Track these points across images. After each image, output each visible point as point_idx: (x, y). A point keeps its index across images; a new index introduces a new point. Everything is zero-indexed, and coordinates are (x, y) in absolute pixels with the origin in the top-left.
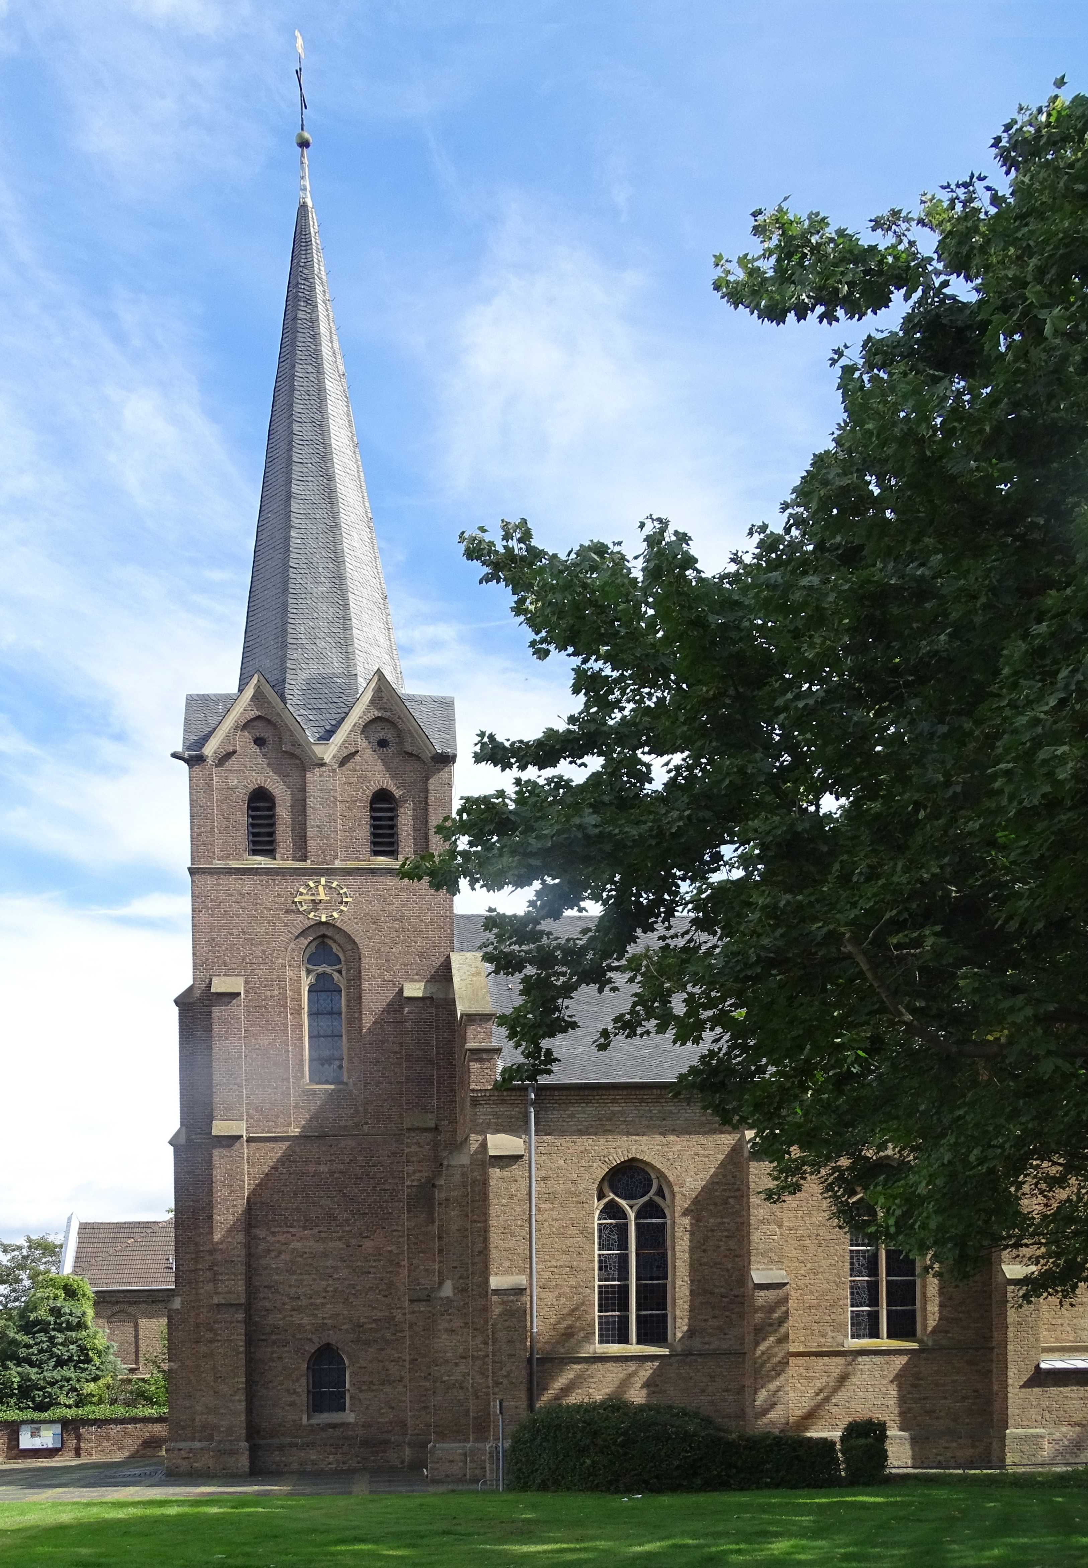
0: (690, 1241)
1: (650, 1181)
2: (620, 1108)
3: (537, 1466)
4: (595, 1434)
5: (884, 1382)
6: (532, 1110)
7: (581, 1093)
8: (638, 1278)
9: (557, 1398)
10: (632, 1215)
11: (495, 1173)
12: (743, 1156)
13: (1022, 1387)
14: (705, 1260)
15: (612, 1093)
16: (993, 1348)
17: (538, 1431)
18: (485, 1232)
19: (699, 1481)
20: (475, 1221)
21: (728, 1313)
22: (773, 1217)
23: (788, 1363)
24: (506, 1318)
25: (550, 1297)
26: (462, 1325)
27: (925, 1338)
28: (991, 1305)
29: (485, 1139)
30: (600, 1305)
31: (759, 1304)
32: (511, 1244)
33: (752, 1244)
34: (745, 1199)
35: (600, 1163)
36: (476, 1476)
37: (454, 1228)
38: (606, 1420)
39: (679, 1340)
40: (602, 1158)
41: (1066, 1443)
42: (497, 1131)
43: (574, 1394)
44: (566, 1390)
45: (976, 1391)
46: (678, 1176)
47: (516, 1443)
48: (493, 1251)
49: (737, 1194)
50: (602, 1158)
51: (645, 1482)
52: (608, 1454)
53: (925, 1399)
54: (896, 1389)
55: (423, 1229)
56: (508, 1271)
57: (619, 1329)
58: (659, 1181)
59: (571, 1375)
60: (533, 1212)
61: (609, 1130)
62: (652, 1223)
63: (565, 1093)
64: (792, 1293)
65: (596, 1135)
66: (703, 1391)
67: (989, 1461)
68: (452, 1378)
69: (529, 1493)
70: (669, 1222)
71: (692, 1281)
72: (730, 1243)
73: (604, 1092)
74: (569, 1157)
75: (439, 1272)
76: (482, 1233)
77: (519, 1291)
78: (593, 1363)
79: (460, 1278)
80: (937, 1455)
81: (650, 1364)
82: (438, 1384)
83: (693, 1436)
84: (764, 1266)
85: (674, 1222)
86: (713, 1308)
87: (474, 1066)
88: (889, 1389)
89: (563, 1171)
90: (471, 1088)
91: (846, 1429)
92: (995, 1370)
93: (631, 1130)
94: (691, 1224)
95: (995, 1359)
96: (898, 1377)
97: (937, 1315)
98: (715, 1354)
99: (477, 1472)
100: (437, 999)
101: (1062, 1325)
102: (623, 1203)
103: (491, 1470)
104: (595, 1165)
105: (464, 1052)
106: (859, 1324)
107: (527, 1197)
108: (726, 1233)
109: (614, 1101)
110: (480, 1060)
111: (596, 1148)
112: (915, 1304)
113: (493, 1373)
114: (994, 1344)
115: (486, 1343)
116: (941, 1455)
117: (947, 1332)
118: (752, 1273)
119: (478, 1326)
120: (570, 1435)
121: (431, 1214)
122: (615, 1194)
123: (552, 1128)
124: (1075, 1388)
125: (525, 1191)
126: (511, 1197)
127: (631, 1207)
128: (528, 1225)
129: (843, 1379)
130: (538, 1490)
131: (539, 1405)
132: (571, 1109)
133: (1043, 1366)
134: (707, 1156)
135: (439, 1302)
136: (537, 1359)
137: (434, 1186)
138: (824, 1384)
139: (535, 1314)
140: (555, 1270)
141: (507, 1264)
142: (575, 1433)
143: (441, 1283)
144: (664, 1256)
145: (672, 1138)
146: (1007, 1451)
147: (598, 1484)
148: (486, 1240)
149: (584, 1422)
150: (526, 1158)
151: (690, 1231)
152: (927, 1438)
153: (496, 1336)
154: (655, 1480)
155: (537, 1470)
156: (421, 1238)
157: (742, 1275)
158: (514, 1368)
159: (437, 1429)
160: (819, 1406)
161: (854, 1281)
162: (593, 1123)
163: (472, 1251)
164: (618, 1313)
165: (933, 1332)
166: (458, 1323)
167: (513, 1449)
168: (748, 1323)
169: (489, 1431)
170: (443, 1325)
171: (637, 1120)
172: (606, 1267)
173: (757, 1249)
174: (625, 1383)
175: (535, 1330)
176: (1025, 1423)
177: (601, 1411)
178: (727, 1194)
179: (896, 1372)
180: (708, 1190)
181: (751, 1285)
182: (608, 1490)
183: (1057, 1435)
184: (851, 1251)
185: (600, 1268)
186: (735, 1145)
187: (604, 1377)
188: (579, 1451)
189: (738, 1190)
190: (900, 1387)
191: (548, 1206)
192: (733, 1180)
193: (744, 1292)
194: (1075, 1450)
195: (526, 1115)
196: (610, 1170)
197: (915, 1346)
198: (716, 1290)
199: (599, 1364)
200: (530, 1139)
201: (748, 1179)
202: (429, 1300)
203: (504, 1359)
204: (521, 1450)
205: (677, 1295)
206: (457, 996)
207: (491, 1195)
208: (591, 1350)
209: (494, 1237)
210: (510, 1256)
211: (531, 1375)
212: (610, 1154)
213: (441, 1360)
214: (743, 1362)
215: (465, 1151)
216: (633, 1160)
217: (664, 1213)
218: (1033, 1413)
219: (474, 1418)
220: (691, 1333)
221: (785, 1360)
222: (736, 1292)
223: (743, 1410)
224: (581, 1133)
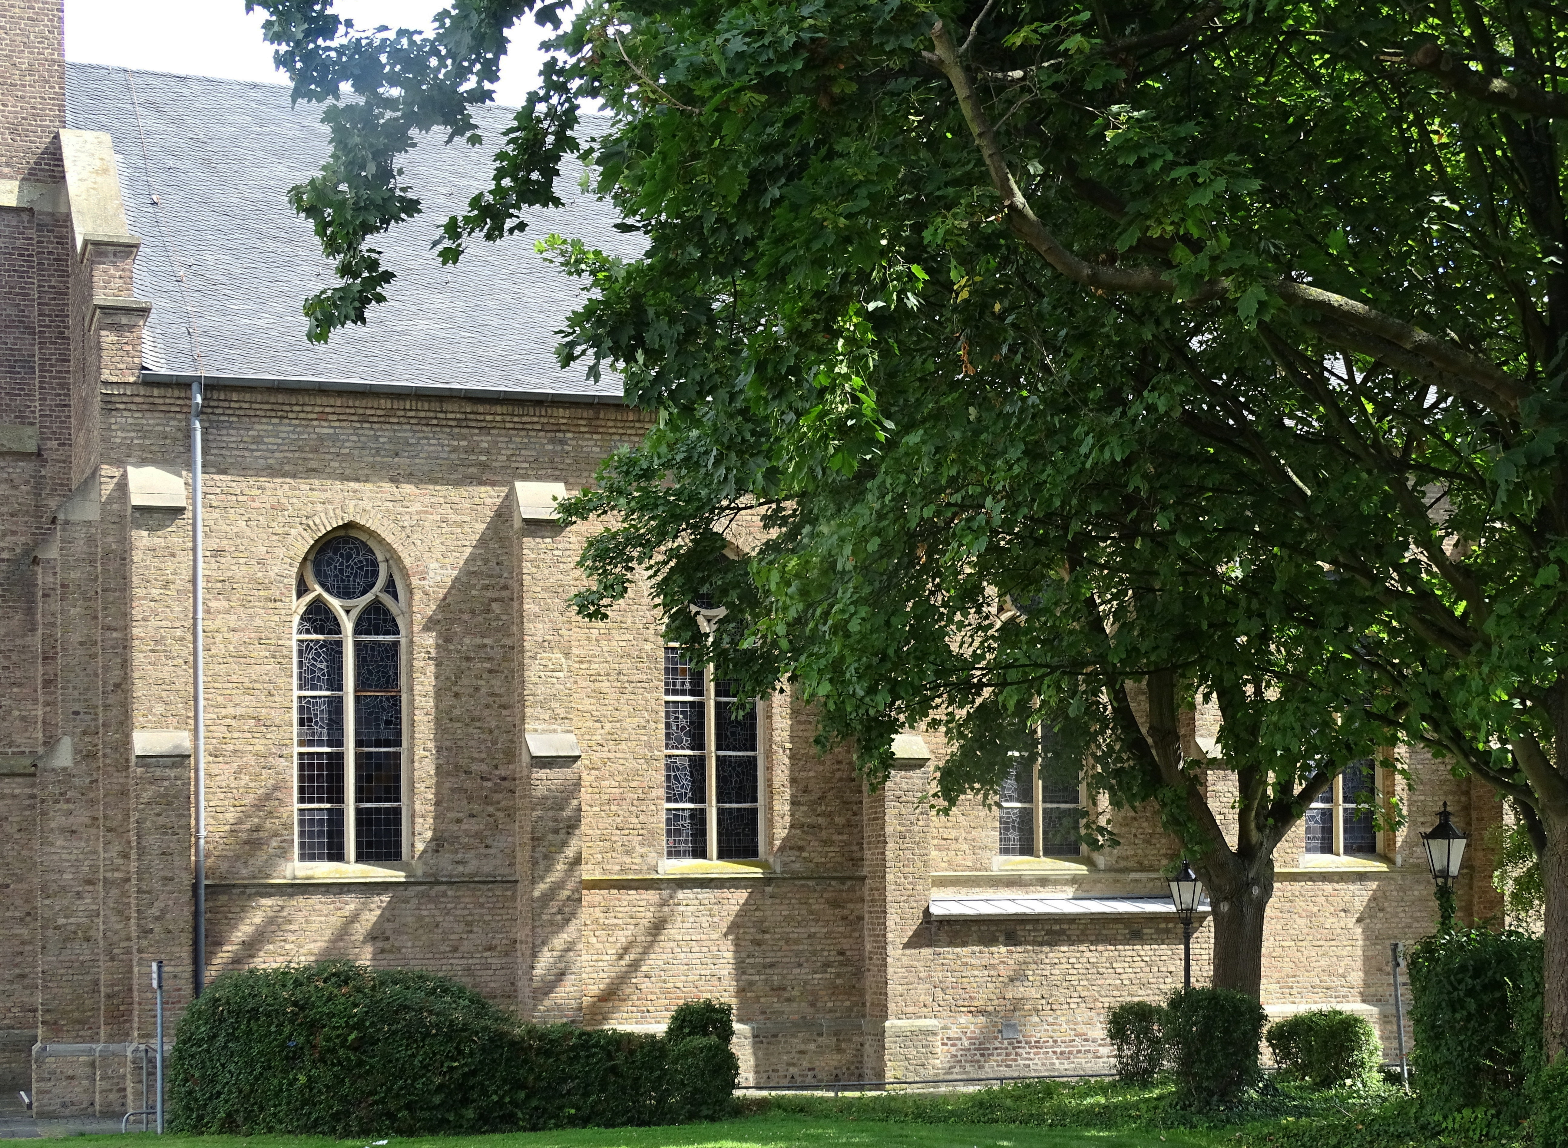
0: (436, 678)
1: (375, 564)
2: (331, 431)
3: (219, 1087)
4: (313, 1026)
5: (715, 936)
6: (198, 424)
7: (273, 400)
8: (359, 743)
9: (236, 961)
10: (348, 625)
11: (141, 538)
12: (512, 526)
13: (907, 946)
14: (457, 712)
15: (319, 401)
16: (863, 879)
17: (222, 1020)
18: (124, 647)
19: (470, 1113)
20: (109, 628)
21: (491, 809)
22: (557, 638)
23: (580, 900)
24: (158, 809)
25: (225, 772)
26: (88, 821)
27: (771, 860)
28: (861, 802)
29: (124, 476)
30: (302, 790)
31: (539, 794)
32: (166, 672)
33: (528, 686)
34: (515, 604)
35: (300, 529)
36: (110, 1105)
37: (75, 638)
38: (329, 999)
39: (420, 858)
40: (304, 521)
41: (966, 1043)
42: (143, 462)
43: (262, 954)
44: (252, 946)
45: (841, 953)
46: (417, 559)
47: (185, 1042)
48: (139, 684)
49: (505, 594)
50: (304, 521)
51: (391, 1116)
52: (333, 1064)
53: (772, 965)
54: (732, 948)
55: (18, 642)
56: (160, 724)
57: (330, 834)
58: (389, 567)
59: (257, 918)
60: (200, 615)
61: (314, 470)
62: (378, 643)
63: (248, 397)
64: (584, 776)
65: (294, 476)
66: (455, 949)
67: (860, 1076)
68: (71, 920)
69: (206, 1137)
70: (403, 641)
71: (439, 749)
72: (493, 682)
73: (306, 399)
74: (254, 516)
75: (44, 722)
76: (120, 650)
77: (179, 759)
78: (291, 895)
79: (84, 733)
80: (790, 1064)
81: (376, 899)
82: (50, 932)
83: (463, 1030)
84: (544, 726)
85: (412, 641)
86: (470, 799)
87: (108, 337)
88: (722, 948)
89: (245, 541)
90: (103, 378)
91: (674, 1019)
92: (867, 916)
93: (348, 472)
94: (438, 646)
95: (867, 898)
96: (734, 927)
97: (788, 819)
98: (471, 882)
99: (112, 1097)
100: (41, 213)
101: (957, 840)
102: (335, 603)
103: (138, 1094)
104: (293, 532)
105: (91, 308)
106: (678, 832)
107: (190, 586)
108: (487, 665)
109: (322, 417)
110: (117, 328)
111: (295, 501)
112: (755, 800)
113: (138, 911)
114: (865, 871)
115: (126, 856)
116: (794, 1065)
117: (801, 849)
118: (528, 736)
119: (115, 824)
120: (273, 1029)
121: (30, 611)
122: (323, 585)
123: (230, 460)
124: (977, 949)
125: (186, 575)
126: (166, 585)
127: (348, 612)
128: (190, 638)
129: (658, 927)
130: (220, 1132)
131: (211, 973)
132: (257, 427)
133: (935, 910)
134: (460, 525)
135: (52, 777)
136: (207, 886)
137: (35, 561)
138: (630, 938)
139: (202, 803)
140: (233, 722)
141: (159, 709)
142: (280, 1025)
143: (50, 743)
144: (396, 702)
145: (408, 489)
146: (886, 1057)
147: (317, 1119)
148: (126, 664)
149: (295, 1004)
150: (188, 514)
151: (435, 659)
152: (775, 1036)
153: (144, 843)
154: (406, 1113)
155: (219, 1094)
156: (14, 658)
157: (512, 741)
158: (171, 903)
159: (48, 1017)
160: (622, 979)
161: (670, 756)
162: (290, 455)
163: (104, 683)
164: (328, 806)
165: (782, 849)
166: (81, 817)
167: (180, 1054)
168: (521, 827)
169: (130, 1021)
170: (57, 821)
171: (356, 452)
172: (310, 720)
173: (534, 695)
174: (343, 933)
175: (203, 833)
176: (910, 1009)
177: (321, 984)
178: (489, 594)
179: (731, 918)
180: (461, 585)
181: (525, 759)
182: (333, 1131)
183: (954, 1032)
184: (667, 702)
185: (302, 723)
186: (500, 507)
187: (307, 922)
188: (287, 1058)
189: (505, 587)
190: (737, 944)
191: (222, 604)
192: (497, 568)
193: (514, 771)
194: (978, 1057)
195: (188, 435)
196: (316, 541)
197: (756, 872)
198: (474, 767)
199: (300, 899)
200: (194, 478)
201: (520, 567)
202: (34, 775)
203: (157, 886)
204: (193, 1056)
205: (417, 774)
206: (73, 209)
207: (134, 579)
208: (288, 874)
209: (140, 659)
210: (164, 694)
211: (196, 915)
212: (316, 513)
213: (55, 887)
214: (514, 898)
215: (93, 496)
216: (350, 526)
217: (396, 625)
218: (921, 991)
219: (108, 996)
220: (438, 843)
221: (577, 896)
222: (502, 772)
223: (513, 984)
224: (273, 472)
